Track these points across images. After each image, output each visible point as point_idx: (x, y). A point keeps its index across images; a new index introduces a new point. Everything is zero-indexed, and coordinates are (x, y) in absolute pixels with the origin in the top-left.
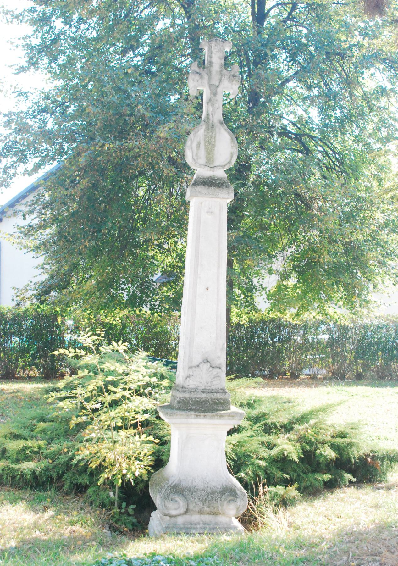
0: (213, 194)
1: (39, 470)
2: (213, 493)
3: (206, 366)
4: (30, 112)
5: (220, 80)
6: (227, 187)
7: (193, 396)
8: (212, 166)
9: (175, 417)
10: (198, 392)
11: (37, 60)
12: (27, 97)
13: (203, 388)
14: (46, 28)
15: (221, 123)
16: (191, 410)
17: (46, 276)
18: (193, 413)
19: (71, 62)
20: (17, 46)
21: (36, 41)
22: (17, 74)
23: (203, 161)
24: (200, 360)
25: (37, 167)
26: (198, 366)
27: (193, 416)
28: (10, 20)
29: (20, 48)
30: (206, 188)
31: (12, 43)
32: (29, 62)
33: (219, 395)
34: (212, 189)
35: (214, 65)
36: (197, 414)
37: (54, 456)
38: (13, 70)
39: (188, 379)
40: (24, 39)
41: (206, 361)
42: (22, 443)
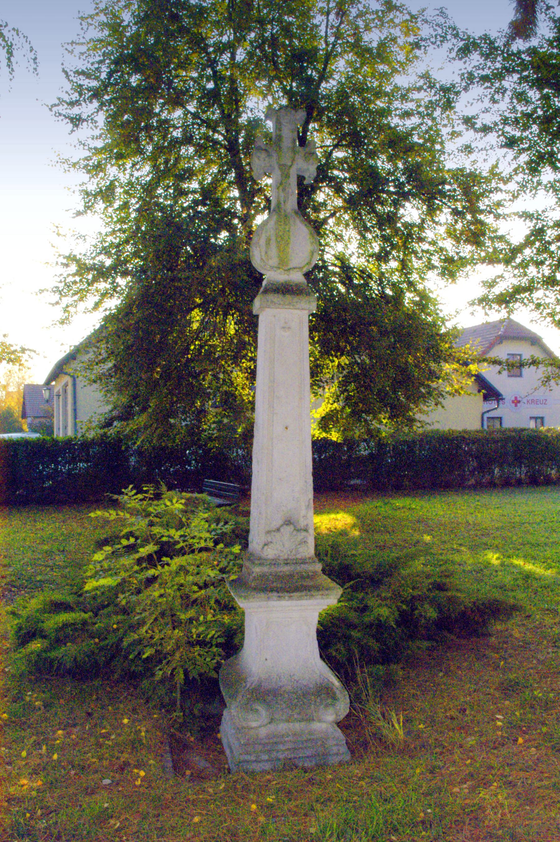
0: (290, 304)
1: (82, 656)
2: (306, 694)
3: (288, 529)
4: (88, 254)
5: (293, 161)
6: (308, 294)
7: (273, 569)
8: (287, 268)
9: (251, 600)
10: (279, 564)
11: (93, 204)
12: (85, 239)
13: (286, 557)
14: (101, 174)
15: (296, 213)
16: (271, 590)
17: (110, 407)
18: (275, 594)
19: (125, 206)
20: (74, 192)
21: (92, 187)
22: (74, 217)
23: (274, 262)
24: (280, 522)
25: (97, 305)
26: (278, 530)
27: (275, 598)
28: (67, 169)
29: (77, 193)
30: (281, 296)
31: (69, 189)
32: (85, 207)
33: (306, 566)
34: (288, 297)
35: (284, 140)
36: (280, 594)
37: (102, 635)
38: (71, 214)
39: (266, 547)
40: (80, 185)
41: (288, 522)
42: (64, 617)
